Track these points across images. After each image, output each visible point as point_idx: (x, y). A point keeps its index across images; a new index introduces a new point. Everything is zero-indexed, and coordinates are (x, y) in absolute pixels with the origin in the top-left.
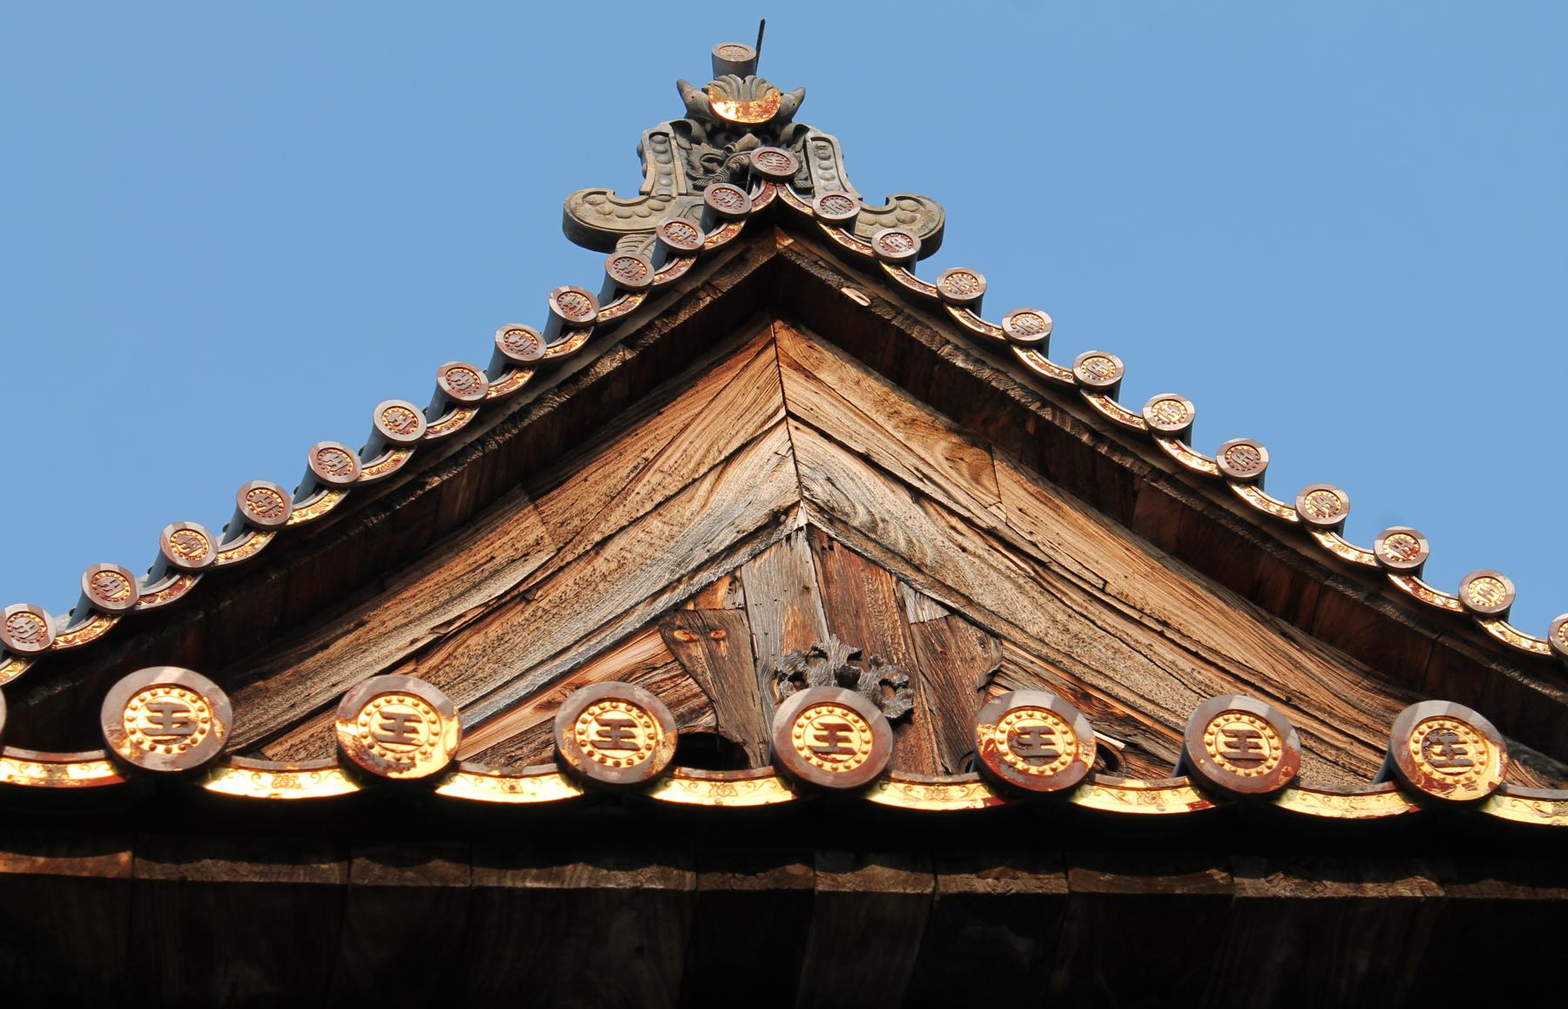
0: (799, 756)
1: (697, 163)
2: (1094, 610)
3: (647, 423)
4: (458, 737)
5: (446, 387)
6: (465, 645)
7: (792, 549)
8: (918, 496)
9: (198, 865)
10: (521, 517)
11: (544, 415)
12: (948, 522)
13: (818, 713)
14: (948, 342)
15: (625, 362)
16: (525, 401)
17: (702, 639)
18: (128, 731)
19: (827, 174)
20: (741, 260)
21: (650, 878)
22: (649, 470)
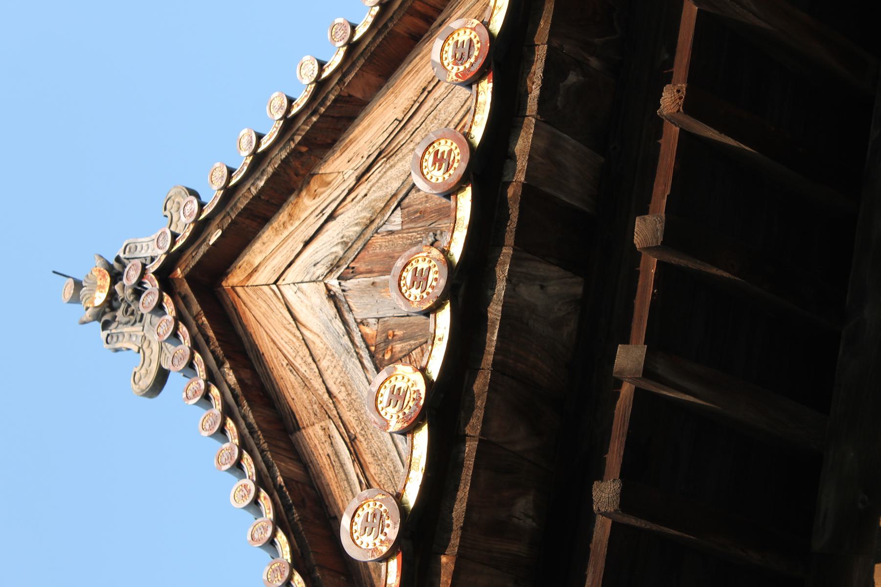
0: (447, 180)
1: (126, 319)
2: (410, 127)
3: (267, 361)
4: (353, 23)
5: (228, 466)
6: (374, 475)
7: (350, 290)
8: (332, 217)
9: (455, 519)
10: (308, 437)
11: (253, 415)
12: (349, 202)
13: (426, 167)
14: (249, 189)
15: (231, 368)
16: (243, 425)
17: (391, 344)
18: (374, 547)
19: (145, 248)
20: (185, 298)
21: (502, 272)
22: (293, 364)
